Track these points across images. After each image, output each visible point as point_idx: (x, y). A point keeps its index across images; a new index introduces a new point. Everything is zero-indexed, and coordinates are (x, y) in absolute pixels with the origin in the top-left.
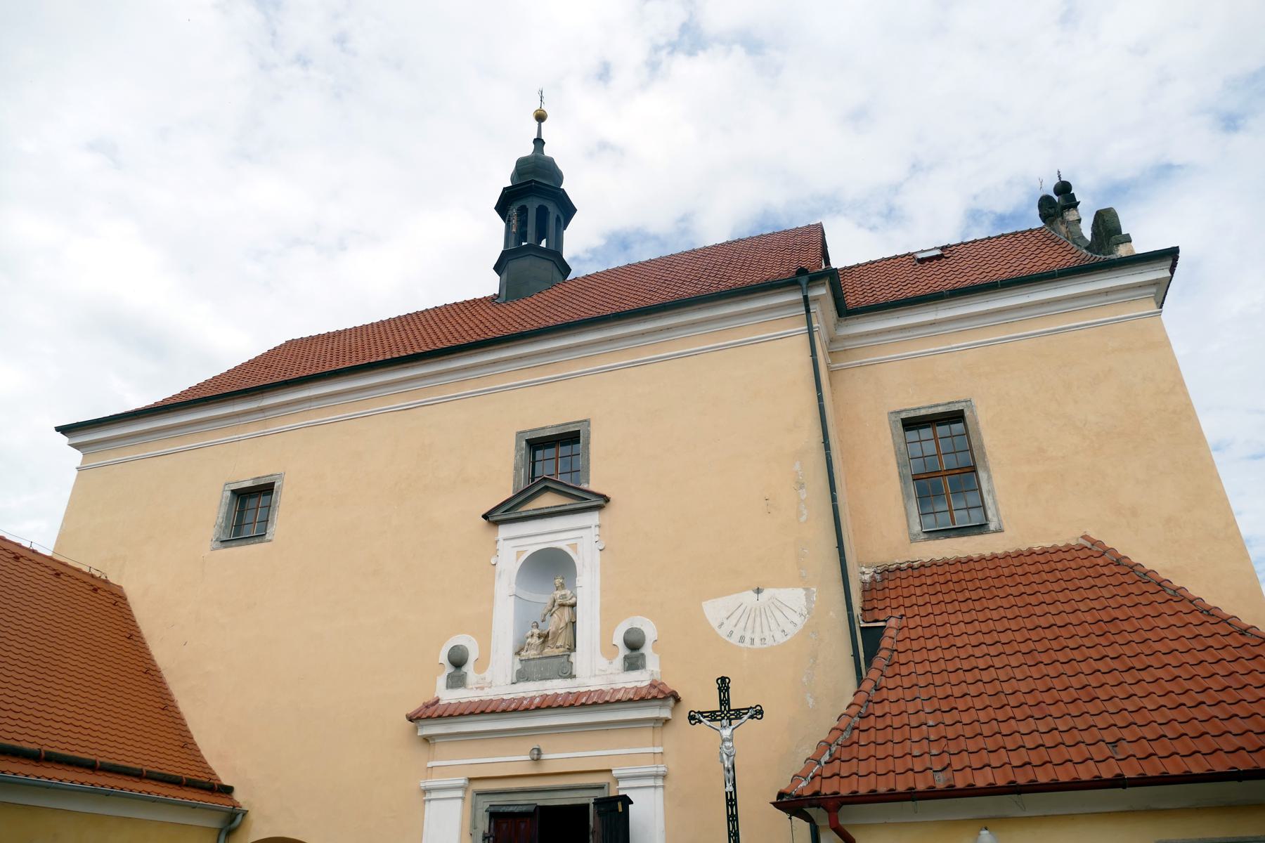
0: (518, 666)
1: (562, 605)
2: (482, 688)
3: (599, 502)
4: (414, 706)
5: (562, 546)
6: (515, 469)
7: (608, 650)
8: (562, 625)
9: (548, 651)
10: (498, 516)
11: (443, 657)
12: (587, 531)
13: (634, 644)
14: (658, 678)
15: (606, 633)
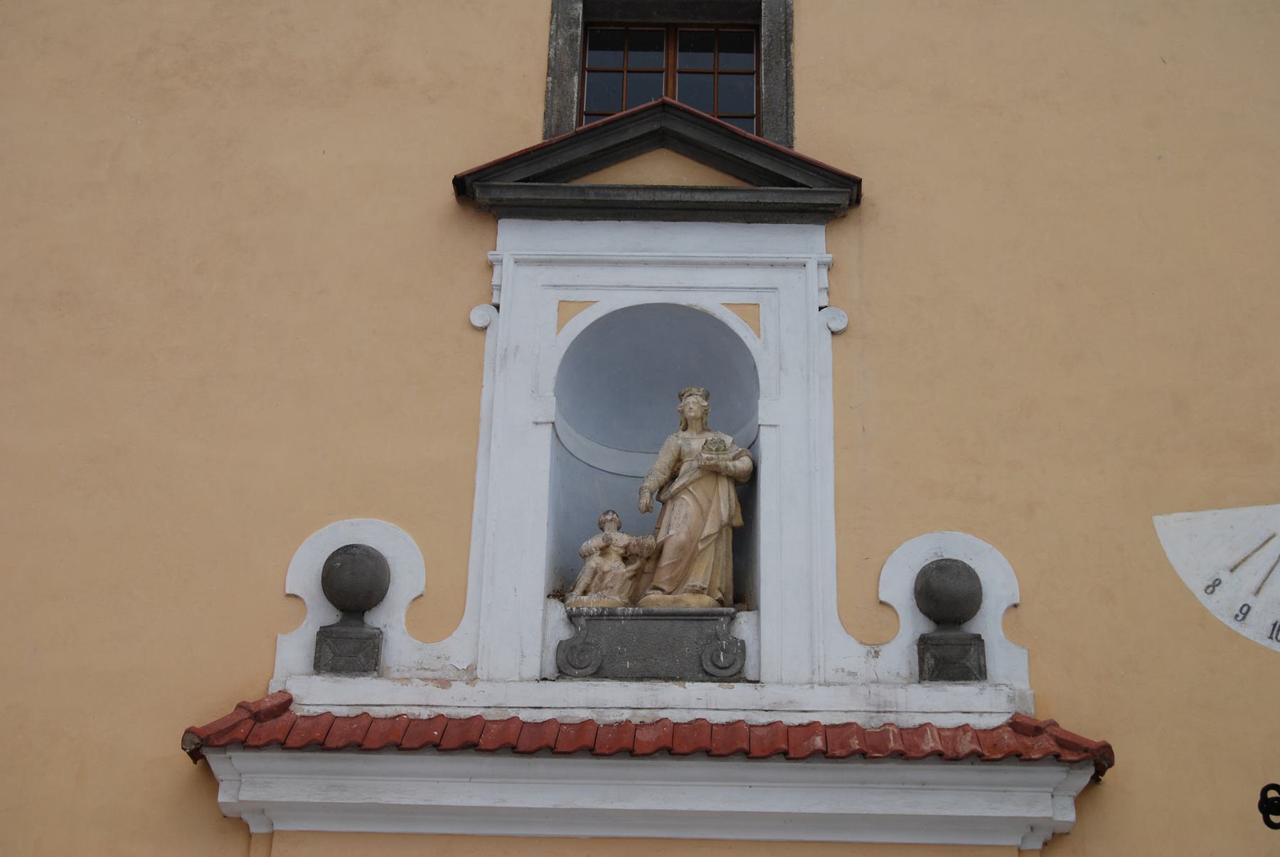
0: (563, 632)
1: (714, 472)
2: (444, 683)
3: (827, 196)
4: (209, 709)
5: (712, 303)
6: (551, 71)
7: (868, 621)
8: (710, 528)
9: (655, 600)
10: (490, 193)
11: (304, 572)
12: (792, 275)
13: (947, 602)
14: (1029, 710)
15: (857, 568)
